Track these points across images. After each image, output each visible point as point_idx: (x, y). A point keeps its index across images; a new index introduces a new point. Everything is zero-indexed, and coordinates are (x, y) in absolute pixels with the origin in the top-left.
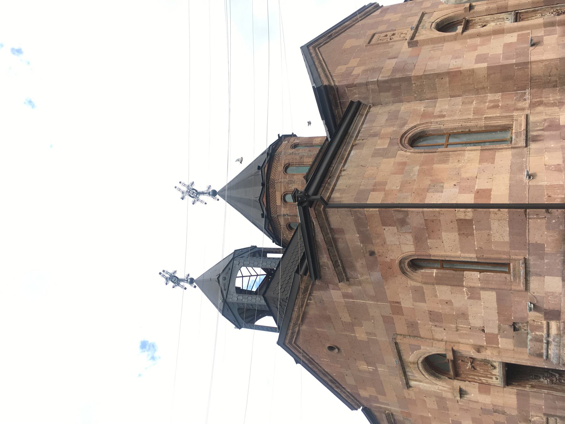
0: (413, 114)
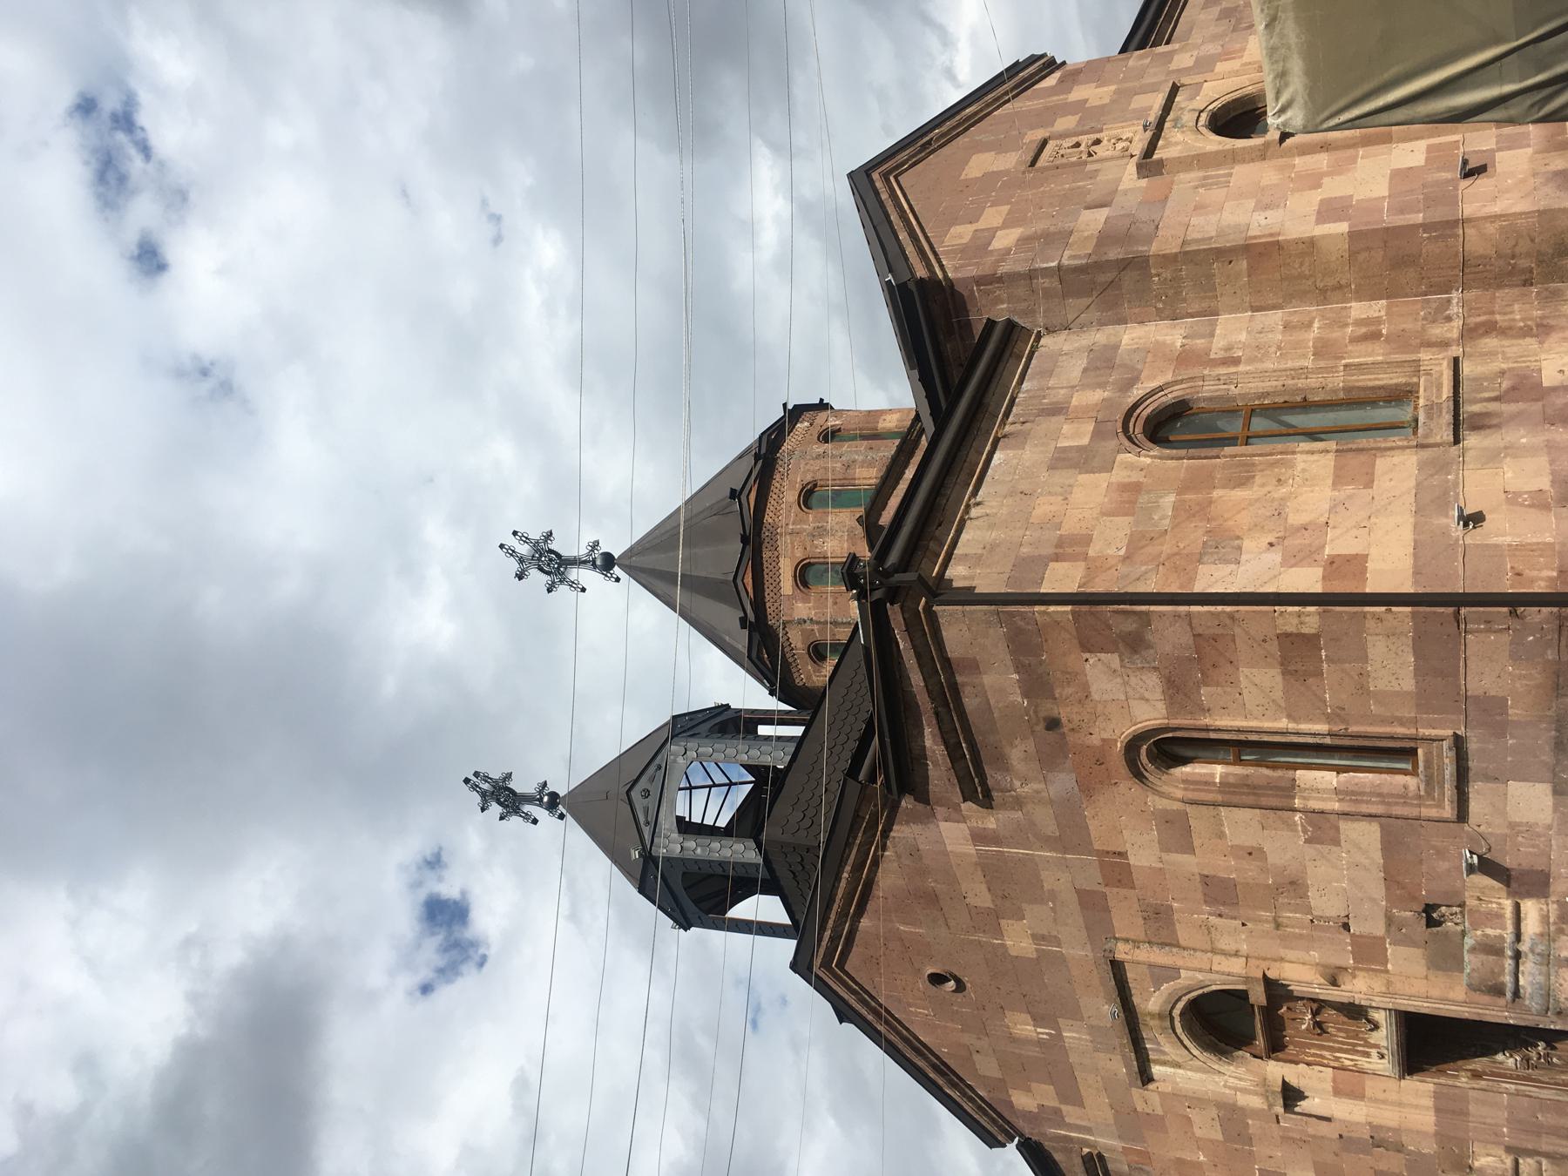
0: (1152, 349)
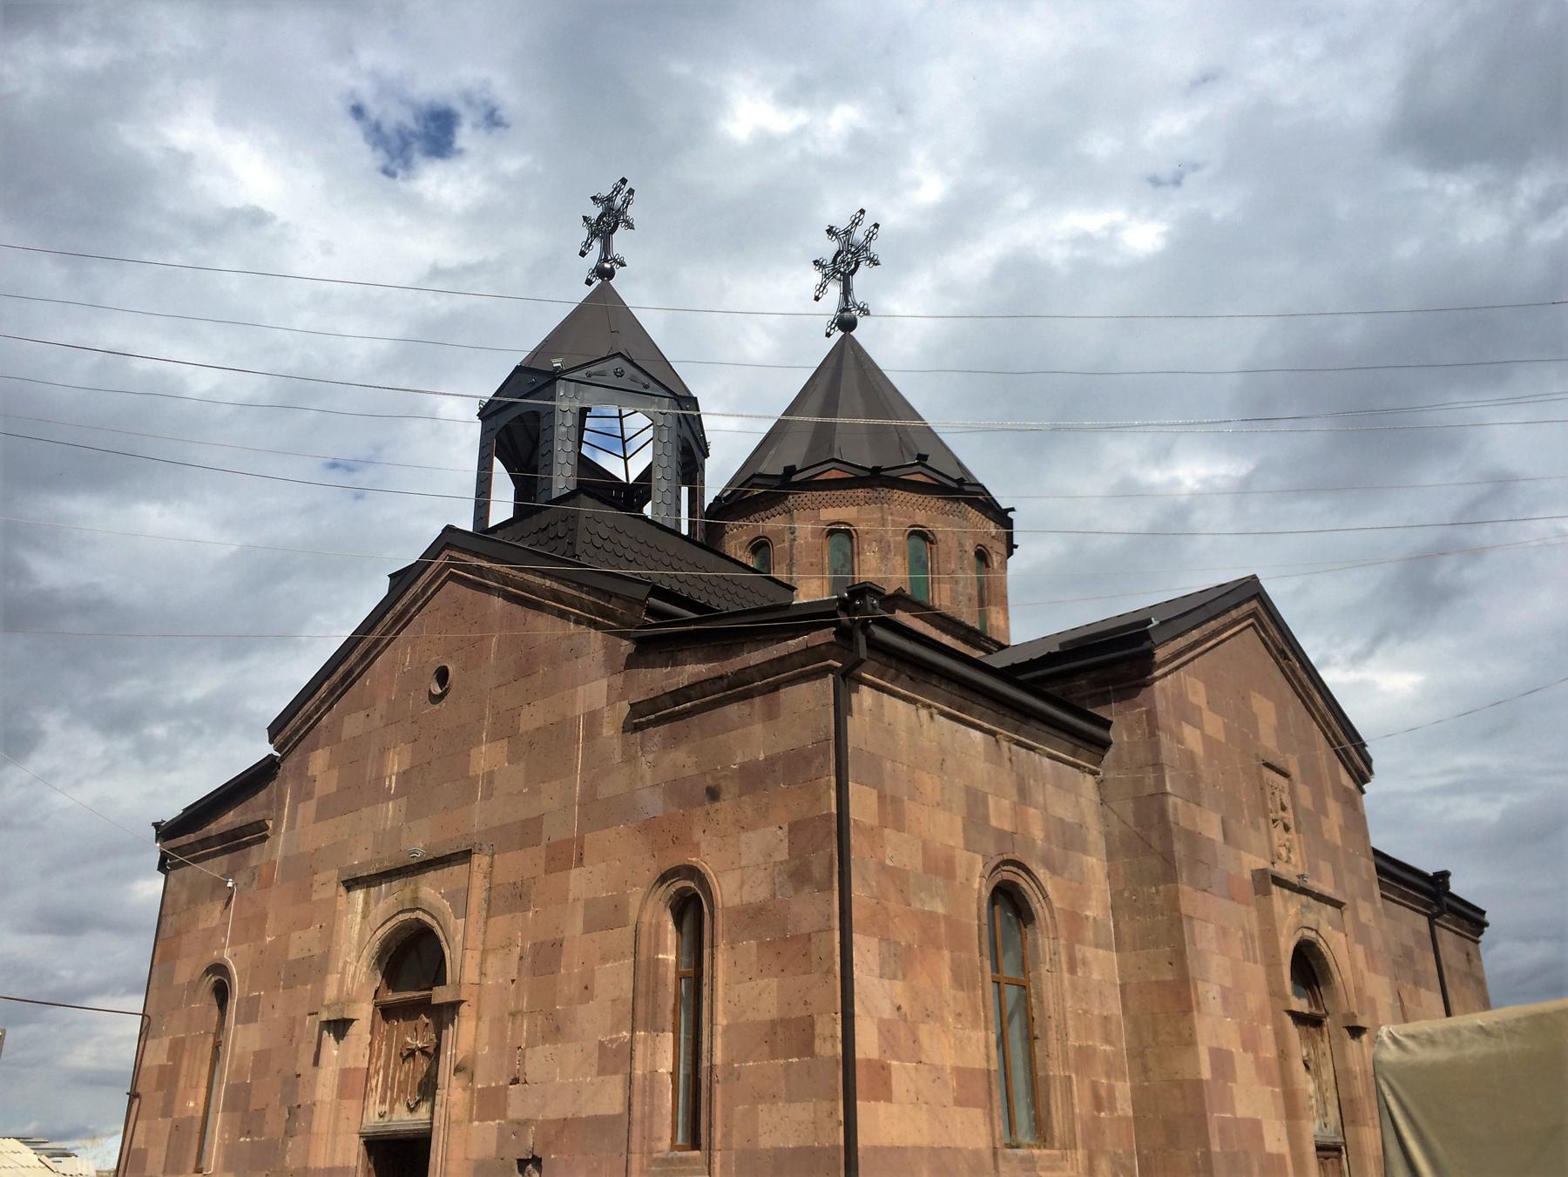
0: (1082, 887)
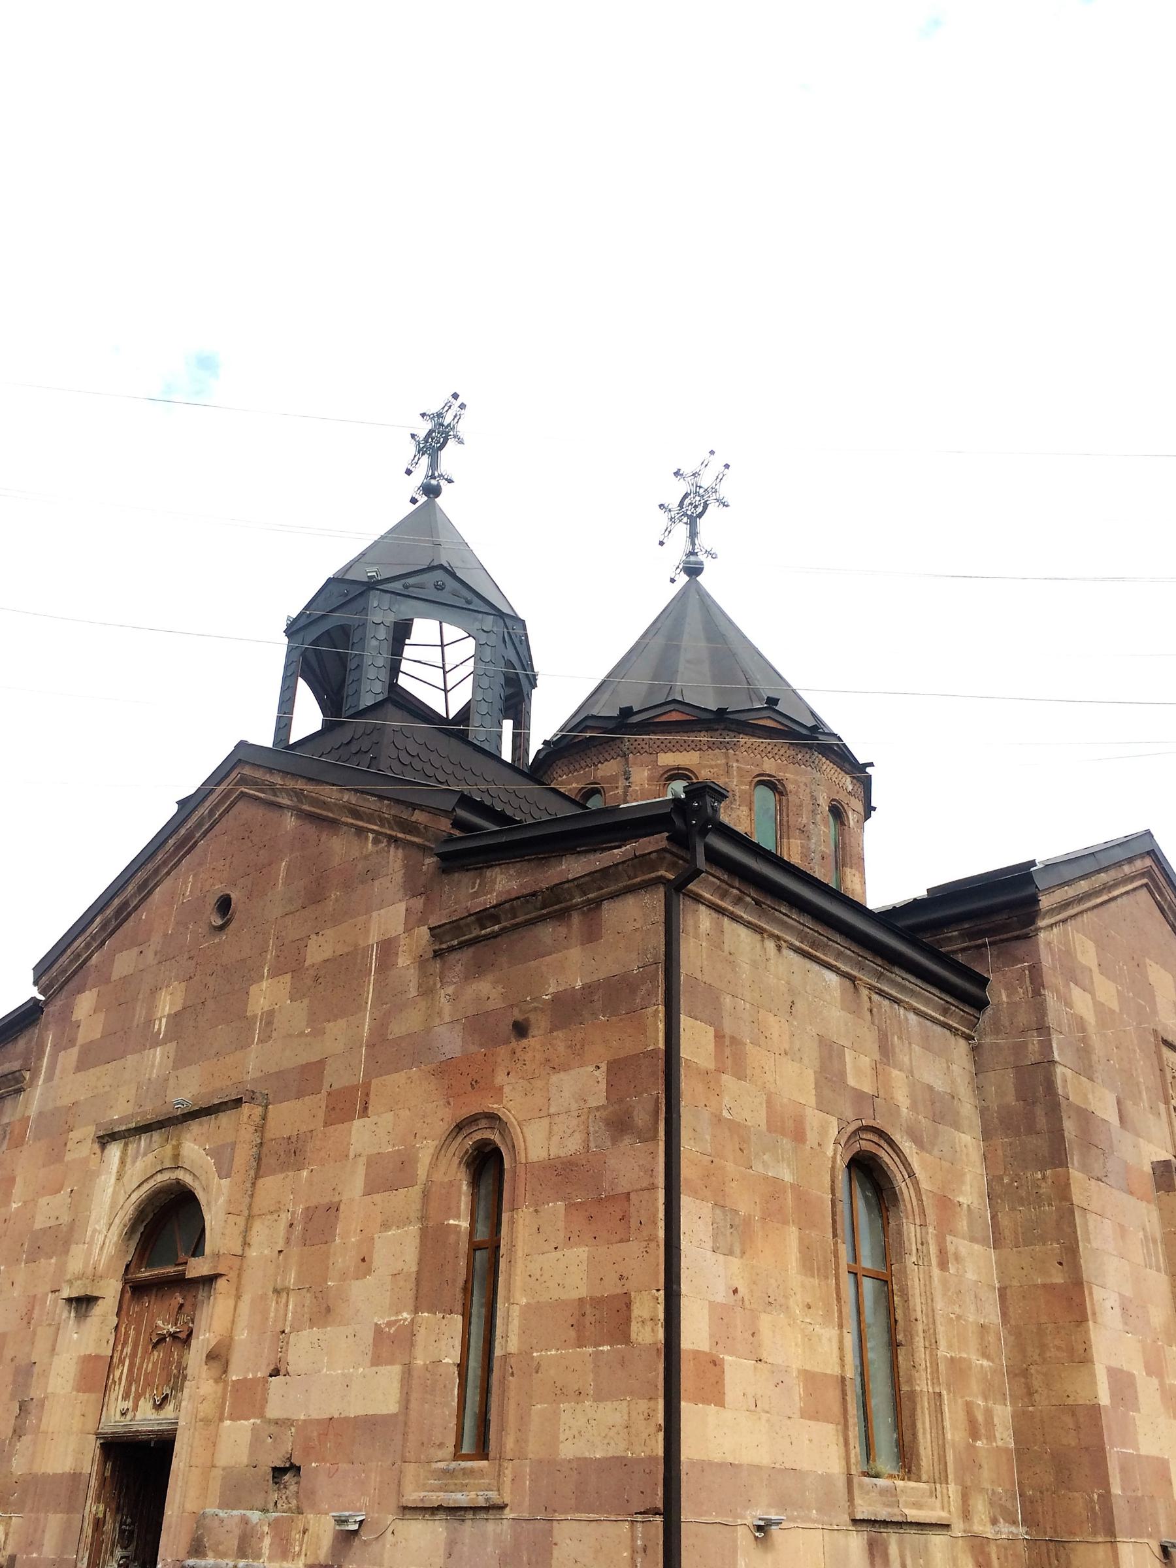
0: (950, 1168)
